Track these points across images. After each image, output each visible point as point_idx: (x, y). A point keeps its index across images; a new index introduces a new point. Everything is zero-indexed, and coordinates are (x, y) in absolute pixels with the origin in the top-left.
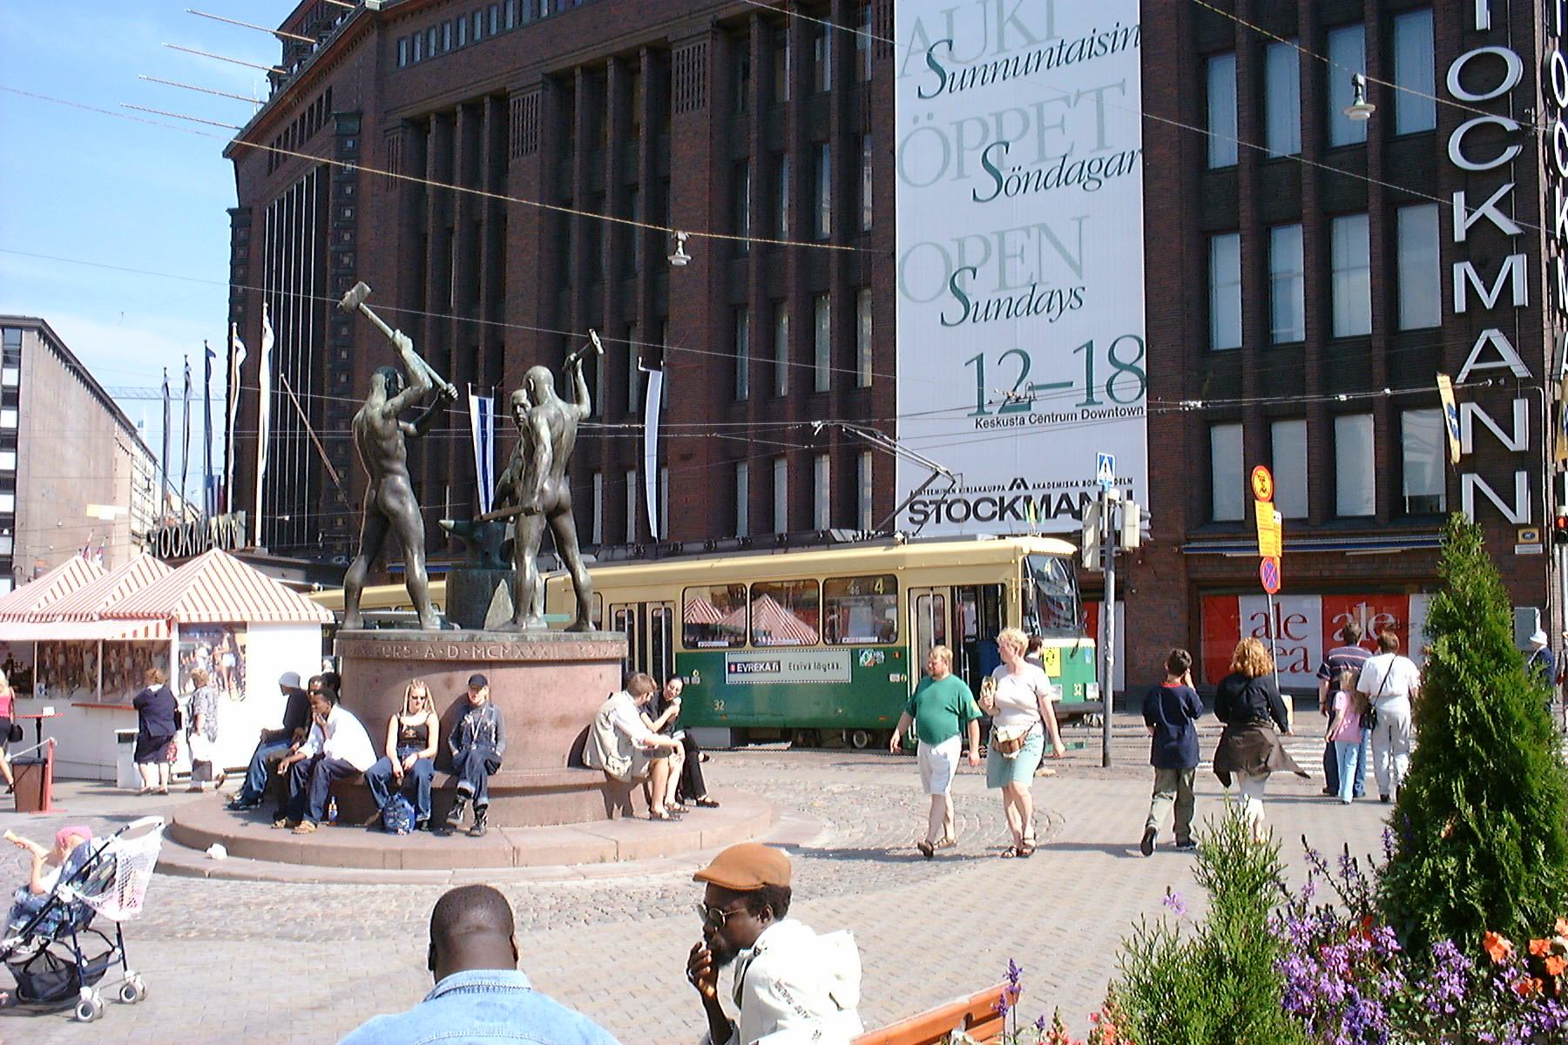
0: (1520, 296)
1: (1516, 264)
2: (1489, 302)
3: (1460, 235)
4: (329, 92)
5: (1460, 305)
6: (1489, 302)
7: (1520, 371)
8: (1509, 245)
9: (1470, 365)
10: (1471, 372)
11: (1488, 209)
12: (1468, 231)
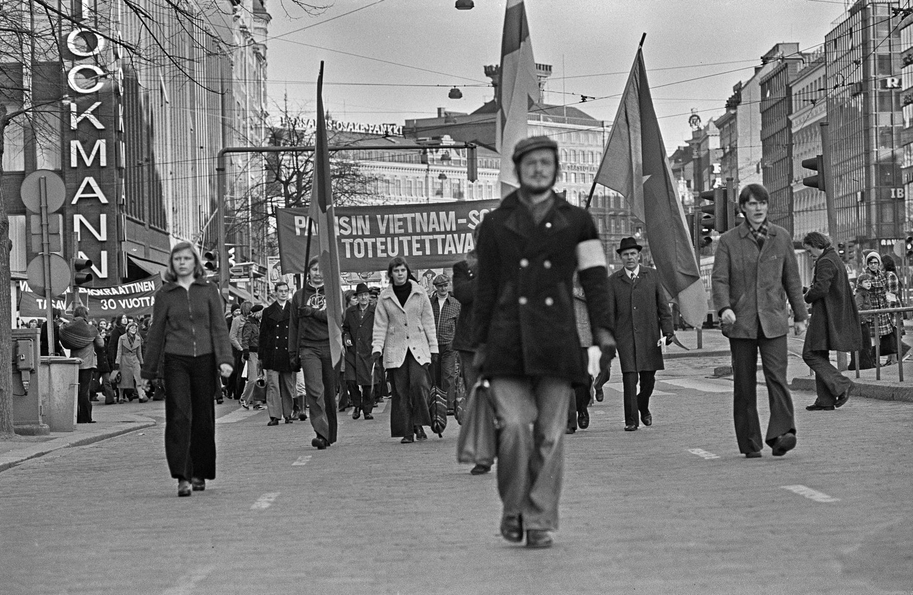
0: (103, 163)
1: (101, 143)
2: (89, 163)
3: (74, 125)
4: (143, 225)
5: (74, 164)
6: (89, 163)
7: (104, 200)
8: (100, 134)
9: (79, 195)
10: (80, 199)
11: (88, 114)
12: (78, 124)
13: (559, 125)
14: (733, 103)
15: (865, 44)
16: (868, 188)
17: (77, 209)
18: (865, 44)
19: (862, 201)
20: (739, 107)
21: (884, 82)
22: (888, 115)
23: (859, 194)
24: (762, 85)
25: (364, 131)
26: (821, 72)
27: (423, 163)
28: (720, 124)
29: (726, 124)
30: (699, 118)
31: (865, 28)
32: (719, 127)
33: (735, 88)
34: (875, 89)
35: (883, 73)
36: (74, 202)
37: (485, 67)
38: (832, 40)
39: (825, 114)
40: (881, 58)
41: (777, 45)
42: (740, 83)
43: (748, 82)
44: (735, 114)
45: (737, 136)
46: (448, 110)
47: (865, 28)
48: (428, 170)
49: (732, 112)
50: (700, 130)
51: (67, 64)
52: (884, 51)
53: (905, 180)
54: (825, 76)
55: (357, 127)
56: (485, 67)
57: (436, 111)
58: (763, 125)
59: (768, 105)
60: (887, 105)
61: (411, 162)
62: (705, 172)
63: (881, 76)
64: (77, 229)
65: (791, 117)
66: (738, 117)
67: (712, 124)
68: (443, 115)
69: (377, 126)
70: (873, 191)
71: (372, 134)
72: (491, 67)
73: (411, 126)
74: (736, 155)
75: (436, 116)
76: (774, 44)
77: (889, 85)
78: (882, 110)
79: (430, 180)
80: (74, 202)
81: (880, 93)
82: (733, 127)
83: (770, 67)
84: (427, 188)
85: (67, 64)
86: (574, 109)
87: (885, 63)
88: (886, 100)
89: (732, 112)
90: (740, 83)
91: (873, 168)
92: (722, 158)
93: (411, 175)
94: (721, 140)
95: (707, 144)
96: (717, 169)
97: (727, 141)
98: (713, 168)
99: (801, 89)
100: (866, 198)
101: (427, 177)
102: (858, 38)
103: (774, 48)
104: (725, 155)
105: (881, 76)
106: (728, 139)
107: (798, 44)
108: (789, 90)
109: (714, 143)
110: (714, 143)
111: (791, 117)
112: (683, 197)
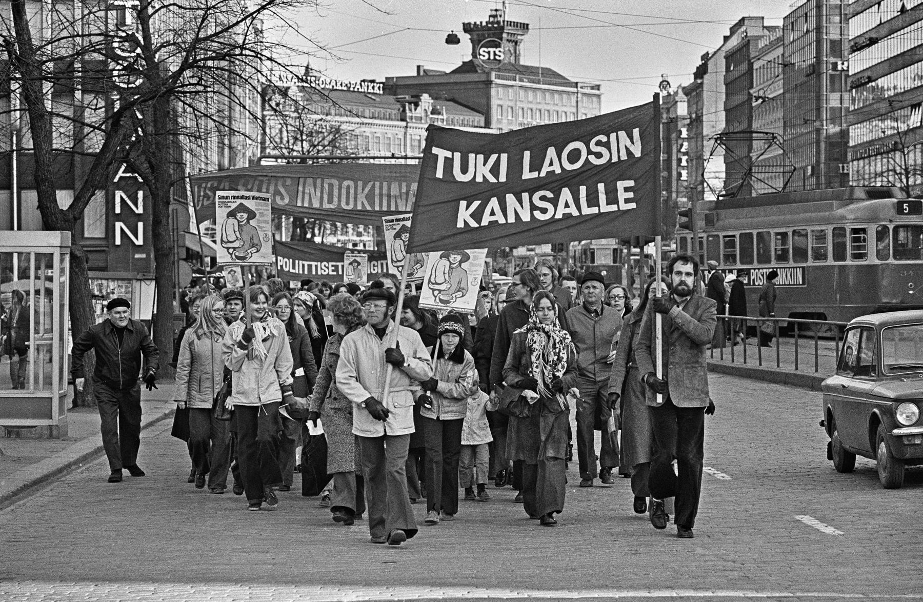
10: (121, 178)
13: (535, 86)
14: (701, 72)
15: (818, 29)
16: (818, 162)
17: (118, 186)
18: (818, 29)
19: (812, 175)
20: (706, 77)
21: (835, 65)
22: (837, 95)
23: (810, 168)
24: (726, 58)
25: (345, 89)
26: (780, 51)
27: (403, 120)
28: (687, 91)
29: (694, 92)
30: (668, 83)
31: (819, 16)
32: (686, 94)
33: (703, 58)
34: (826, 72)
35: (835, 57)
36: (116, 180)
37: (464, 24)
38: (791, 21)
39: (782, 91)
40: (832, 42)
41: (743, 19)
42: (707, 53)
43: (715, 53)
44: (702, 83)
45: (703, 104)
46: (426, 68)
47: (819, 16)
48: (407, 127)
49: (699, 81)
50: (669, 94)
51: (112, 65)
52: (834, 35)
53: (849, 157)
54: (783, 55)
55: (339, 84)
56: (464, 24)
57: (416, 69)
58: (727, 94)
59: (731, 78)
60: (837, 85)
61: (390, 119)
62: (674, 136)
63: (832, 60)
64: (118, 200)
65: (751, 91)
66: (705, 87)
67: (680, 91)
68: (422, 73)
69: (359, 83)
70: (822, 166)
71: (354, 91)
72: (470, 24)
73: (391, 83)
74: (702, 121)
75: (415, 74)
76: (740, 18)
77: (839, 68)
78: (833, 91)
79: (408, 137)
80: (116, 180)
81: (831, 75)
82: (699, 96)
83: (734, 42)
84: (405, 145)
85: (112, 65)
86: (550, 70)
87: (836, 48)
88: (837, 81)
89: (699, 81)
90: (707, 53)
91: (823, 145)
92: (688, 125)
93: (390, 133)
94: (689, 106)
95: (676, 110)
96: (684, 134)
97: (694, 108)
98: (681, 132)
99: (776, 56)
100: (816, 172)
101: (405, 133)
102: (812, 24)
103: (740, 21)
104: (691, 122)
105: (832, 60)
106: (695, 106)
107: (763, 18)
108: (751, 65)
109: (682, 109)
110: (682, 109)
111: (751, 91)
112: (315, 426)
